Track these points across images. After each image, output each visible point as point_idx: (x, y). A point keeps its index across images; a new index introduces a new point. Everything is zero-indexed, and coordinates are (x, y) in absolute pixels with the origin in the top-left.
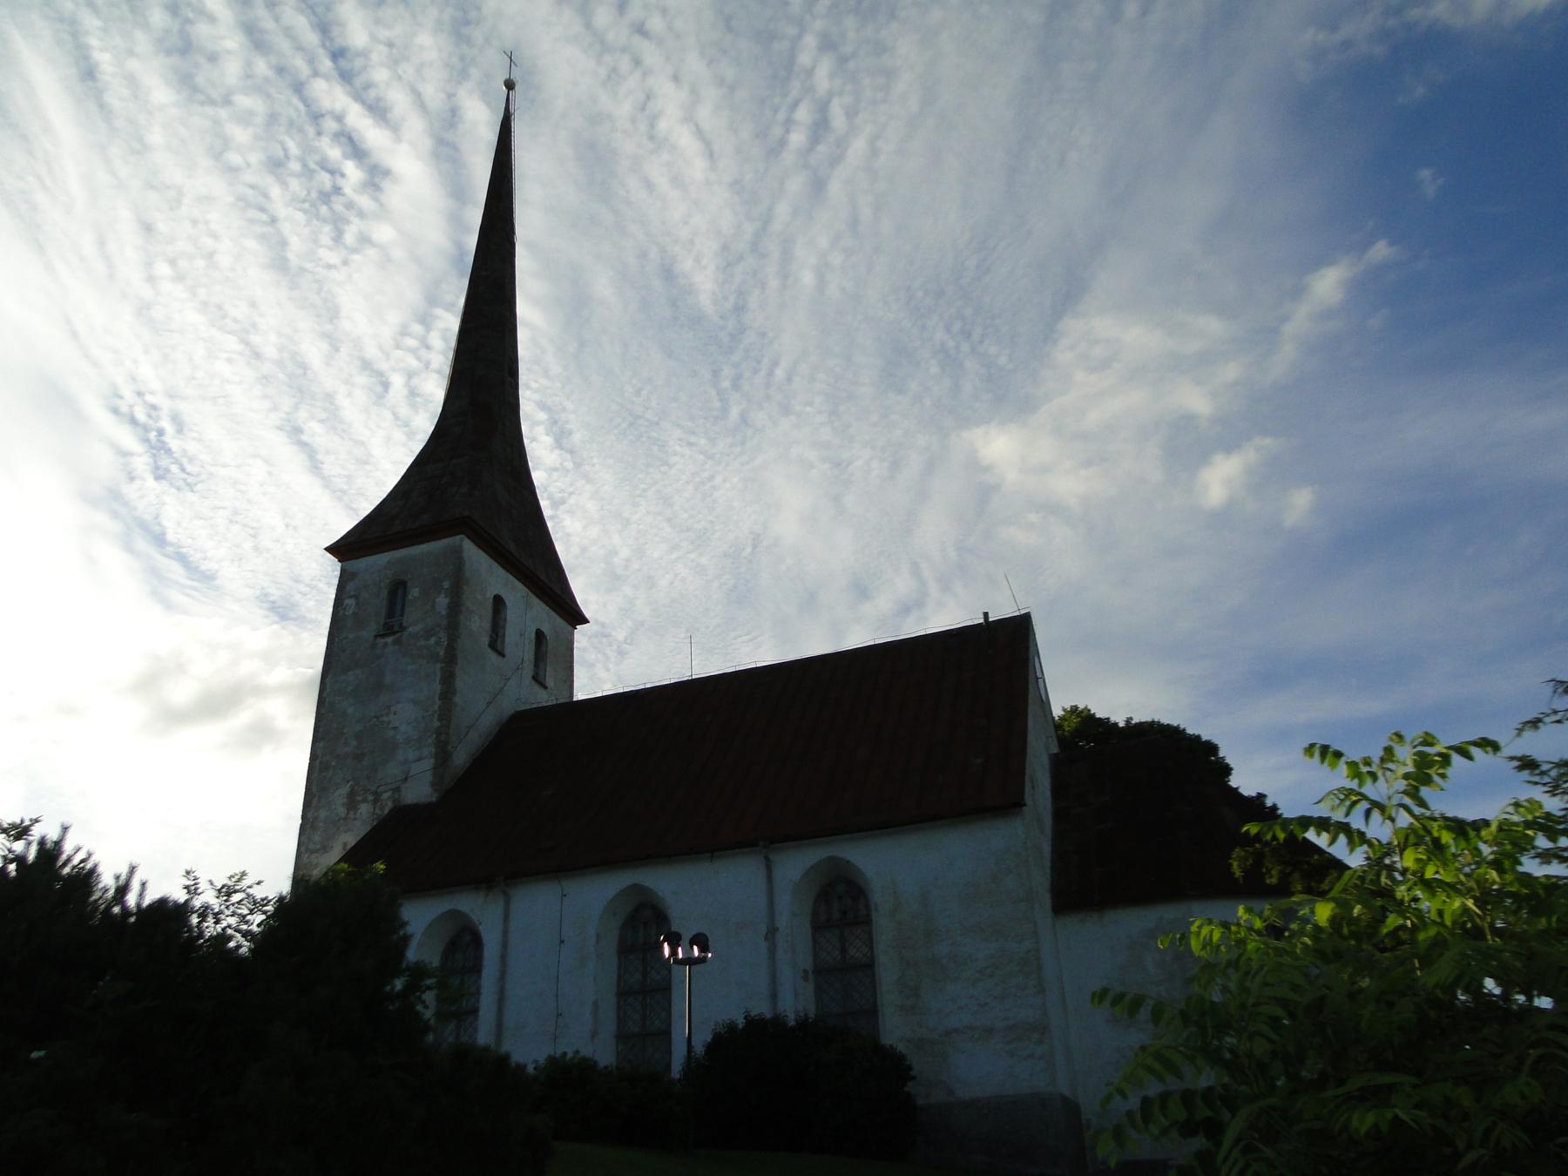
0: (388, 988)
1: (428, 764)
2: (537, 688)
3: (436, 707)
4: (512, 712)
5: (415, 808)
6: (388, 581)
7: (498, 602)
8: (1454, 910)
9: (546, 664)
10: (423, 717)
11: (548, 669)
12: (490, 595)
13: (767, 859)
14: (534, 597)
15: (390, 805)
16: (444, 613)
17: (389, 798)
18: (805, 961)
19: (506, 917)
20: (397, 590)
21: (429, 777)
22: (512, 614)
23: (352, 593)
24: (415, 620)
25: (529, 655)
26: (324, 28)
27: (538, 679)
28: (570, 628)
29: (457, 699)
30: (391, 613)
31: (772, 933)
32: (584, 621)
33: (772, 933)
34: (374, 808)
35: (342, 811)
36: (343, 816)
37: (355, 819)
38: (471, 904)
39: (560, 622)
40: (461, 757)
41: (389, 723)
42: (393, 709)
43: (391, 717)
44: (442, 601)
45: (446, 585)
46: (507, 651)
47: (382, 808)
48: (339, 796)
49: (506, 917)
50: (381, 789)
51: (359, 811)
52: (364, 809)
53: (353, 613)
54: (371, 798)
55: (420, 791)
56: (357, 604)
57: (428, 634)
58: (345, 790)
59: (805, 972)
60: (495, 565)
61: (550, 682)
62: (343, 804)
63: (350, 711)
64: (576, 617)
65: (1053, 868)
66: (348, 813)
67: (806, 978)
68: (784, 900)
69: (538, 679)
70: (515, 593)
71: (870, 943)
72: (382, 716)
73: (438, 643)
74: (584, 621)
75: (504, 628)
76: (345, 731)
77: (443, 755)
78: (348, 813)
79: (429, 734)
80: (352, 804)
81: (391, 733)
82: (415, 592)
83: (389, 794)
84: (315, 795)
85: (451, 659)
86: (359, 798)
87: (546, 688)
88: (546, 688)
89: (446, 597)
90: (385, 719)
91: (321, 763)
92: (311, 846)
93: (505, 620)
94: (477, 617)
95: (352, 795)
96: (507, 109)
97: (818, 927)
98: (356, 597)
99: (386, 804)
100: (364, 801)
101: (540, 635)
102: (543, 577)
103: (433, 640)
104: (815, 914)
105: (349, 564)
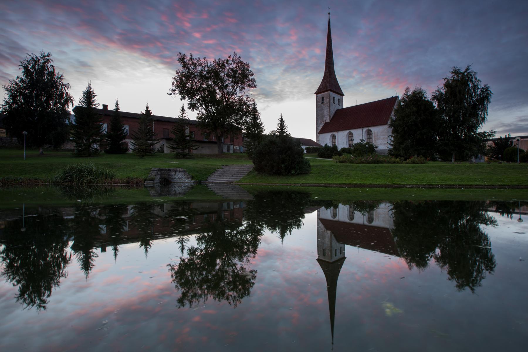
1: (328, 118)
5: (327, 122)
7: (334, 97)
8: (217, 294)
13: (362, 129)
19: (338, 134)
20: (323, 98)
21: (329, 119)
24: (325, 101)
25: (338, 102)
26: (322, 187)
29: (331, 110)
30: (322, 101)
31: (363, 135)
32: (317, 260)
33: (363, 135)
38: (334, 133)
39: (341, 96)
40: (331, 117)
44: (328, 99)
45: (328, 97)
48: (320, 121)
49: (338, 134)
52: (322, 122)
55: (328, 121)
58: (320, 121)
61: (340, 104)
64: (318, 260)
68: (364, 133)
71: (372, 136)
74: (317, 260)
77: (330, 117)
82: (325, 98)
85: (330, 106)
95: (321, 121)
96: (329, 19)
97: (367, 135)
101: (339, 99)
104: (367, 134)
105: (317, 95)
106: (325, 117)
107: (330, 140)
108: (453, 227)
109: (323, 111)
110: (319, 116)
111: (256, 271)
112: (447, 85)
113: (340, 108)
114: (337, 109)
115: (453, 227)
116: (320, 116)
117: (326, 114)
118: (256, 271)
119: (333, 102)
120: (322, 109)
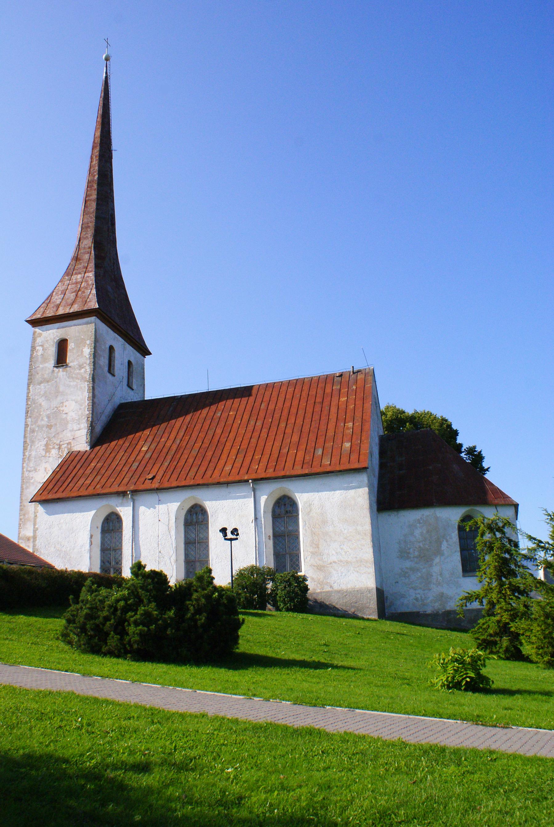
0: (437, 432)
2: (129, 390)
3: (86, 404)
4: (119, 404)
6: (58, 339)
7: (111, 348)
9: (132, 378)
10: (80, 409)
11: (134, 380)
12: (108, 346)
14: (126, 344)
15: (66, 452)
16: (88, 357)
17: (65, 447)
18: (270, 532)
22: (117, 354)
23: (40, 344)
27: (130, 386)
28: (142, 357)
32: (149, 353)
34: (59, 452)
35: (43, 453)
36: (44, 455)
37: (49, 457)
39: (138, 355)
41: (63, 411)
42: (65, 404)
43: (64, 408)
46: (116, 374)
47: (63, 452)
50: (61, 443)
51: (51, 453)
52: (54, 452)
53: (42, 354)
54: (57, 447)
56: (43, 350)
57: (81, 367)
58: (44, 442)
59: (269, 536)
60: (109, 330)
61: (134, 387)
62: (43, 449)
63: (43, 404)
64: (145, 352)
65: (378, 491)
66: (46, 454)
67: (269, 539)
69: (130, 386)
70: (118, 342)
72: (59, 407)
73: (86, 372)
74: (149, 353)
75: (114, 361)
76: (41, 413)
78: (46, 454)
79: (84, 417)
80: (47, 449)
81: (65, 416)
83: (66, 445)
84: (29, 445)
86: (51, 447)
87: (133, 390)
88: (133, 390)
89: (88, 349)
90: (62, 409)
91: (30, 428)
92: (29, 469)
93: (114, 357)
94: (102, 358)
95: (47, 445)
98: (42, 346)
99: (64, 450)
100: (54, 448)
101: (130, 363)
102: (131, 333)
103: (83, 370)
106: (70, 426)
107: (91, 537)
108: (214, 596)
109: (59, 398)
110: (40, 423)
111: (220, 531)
112: (111, 657)
113: (132, 397)
114: (123, 401)
115: (214, 596)
116: (45, 421)
117: (72, 415)
118: (220, 531)
119: (106, 369)
120: (57, 392)
